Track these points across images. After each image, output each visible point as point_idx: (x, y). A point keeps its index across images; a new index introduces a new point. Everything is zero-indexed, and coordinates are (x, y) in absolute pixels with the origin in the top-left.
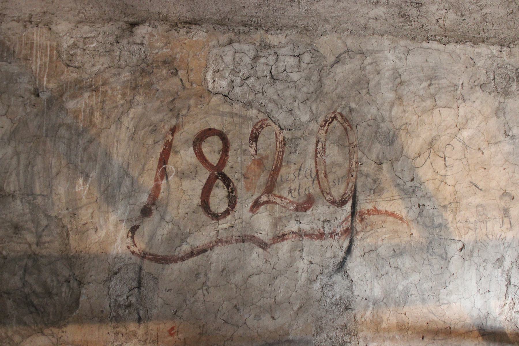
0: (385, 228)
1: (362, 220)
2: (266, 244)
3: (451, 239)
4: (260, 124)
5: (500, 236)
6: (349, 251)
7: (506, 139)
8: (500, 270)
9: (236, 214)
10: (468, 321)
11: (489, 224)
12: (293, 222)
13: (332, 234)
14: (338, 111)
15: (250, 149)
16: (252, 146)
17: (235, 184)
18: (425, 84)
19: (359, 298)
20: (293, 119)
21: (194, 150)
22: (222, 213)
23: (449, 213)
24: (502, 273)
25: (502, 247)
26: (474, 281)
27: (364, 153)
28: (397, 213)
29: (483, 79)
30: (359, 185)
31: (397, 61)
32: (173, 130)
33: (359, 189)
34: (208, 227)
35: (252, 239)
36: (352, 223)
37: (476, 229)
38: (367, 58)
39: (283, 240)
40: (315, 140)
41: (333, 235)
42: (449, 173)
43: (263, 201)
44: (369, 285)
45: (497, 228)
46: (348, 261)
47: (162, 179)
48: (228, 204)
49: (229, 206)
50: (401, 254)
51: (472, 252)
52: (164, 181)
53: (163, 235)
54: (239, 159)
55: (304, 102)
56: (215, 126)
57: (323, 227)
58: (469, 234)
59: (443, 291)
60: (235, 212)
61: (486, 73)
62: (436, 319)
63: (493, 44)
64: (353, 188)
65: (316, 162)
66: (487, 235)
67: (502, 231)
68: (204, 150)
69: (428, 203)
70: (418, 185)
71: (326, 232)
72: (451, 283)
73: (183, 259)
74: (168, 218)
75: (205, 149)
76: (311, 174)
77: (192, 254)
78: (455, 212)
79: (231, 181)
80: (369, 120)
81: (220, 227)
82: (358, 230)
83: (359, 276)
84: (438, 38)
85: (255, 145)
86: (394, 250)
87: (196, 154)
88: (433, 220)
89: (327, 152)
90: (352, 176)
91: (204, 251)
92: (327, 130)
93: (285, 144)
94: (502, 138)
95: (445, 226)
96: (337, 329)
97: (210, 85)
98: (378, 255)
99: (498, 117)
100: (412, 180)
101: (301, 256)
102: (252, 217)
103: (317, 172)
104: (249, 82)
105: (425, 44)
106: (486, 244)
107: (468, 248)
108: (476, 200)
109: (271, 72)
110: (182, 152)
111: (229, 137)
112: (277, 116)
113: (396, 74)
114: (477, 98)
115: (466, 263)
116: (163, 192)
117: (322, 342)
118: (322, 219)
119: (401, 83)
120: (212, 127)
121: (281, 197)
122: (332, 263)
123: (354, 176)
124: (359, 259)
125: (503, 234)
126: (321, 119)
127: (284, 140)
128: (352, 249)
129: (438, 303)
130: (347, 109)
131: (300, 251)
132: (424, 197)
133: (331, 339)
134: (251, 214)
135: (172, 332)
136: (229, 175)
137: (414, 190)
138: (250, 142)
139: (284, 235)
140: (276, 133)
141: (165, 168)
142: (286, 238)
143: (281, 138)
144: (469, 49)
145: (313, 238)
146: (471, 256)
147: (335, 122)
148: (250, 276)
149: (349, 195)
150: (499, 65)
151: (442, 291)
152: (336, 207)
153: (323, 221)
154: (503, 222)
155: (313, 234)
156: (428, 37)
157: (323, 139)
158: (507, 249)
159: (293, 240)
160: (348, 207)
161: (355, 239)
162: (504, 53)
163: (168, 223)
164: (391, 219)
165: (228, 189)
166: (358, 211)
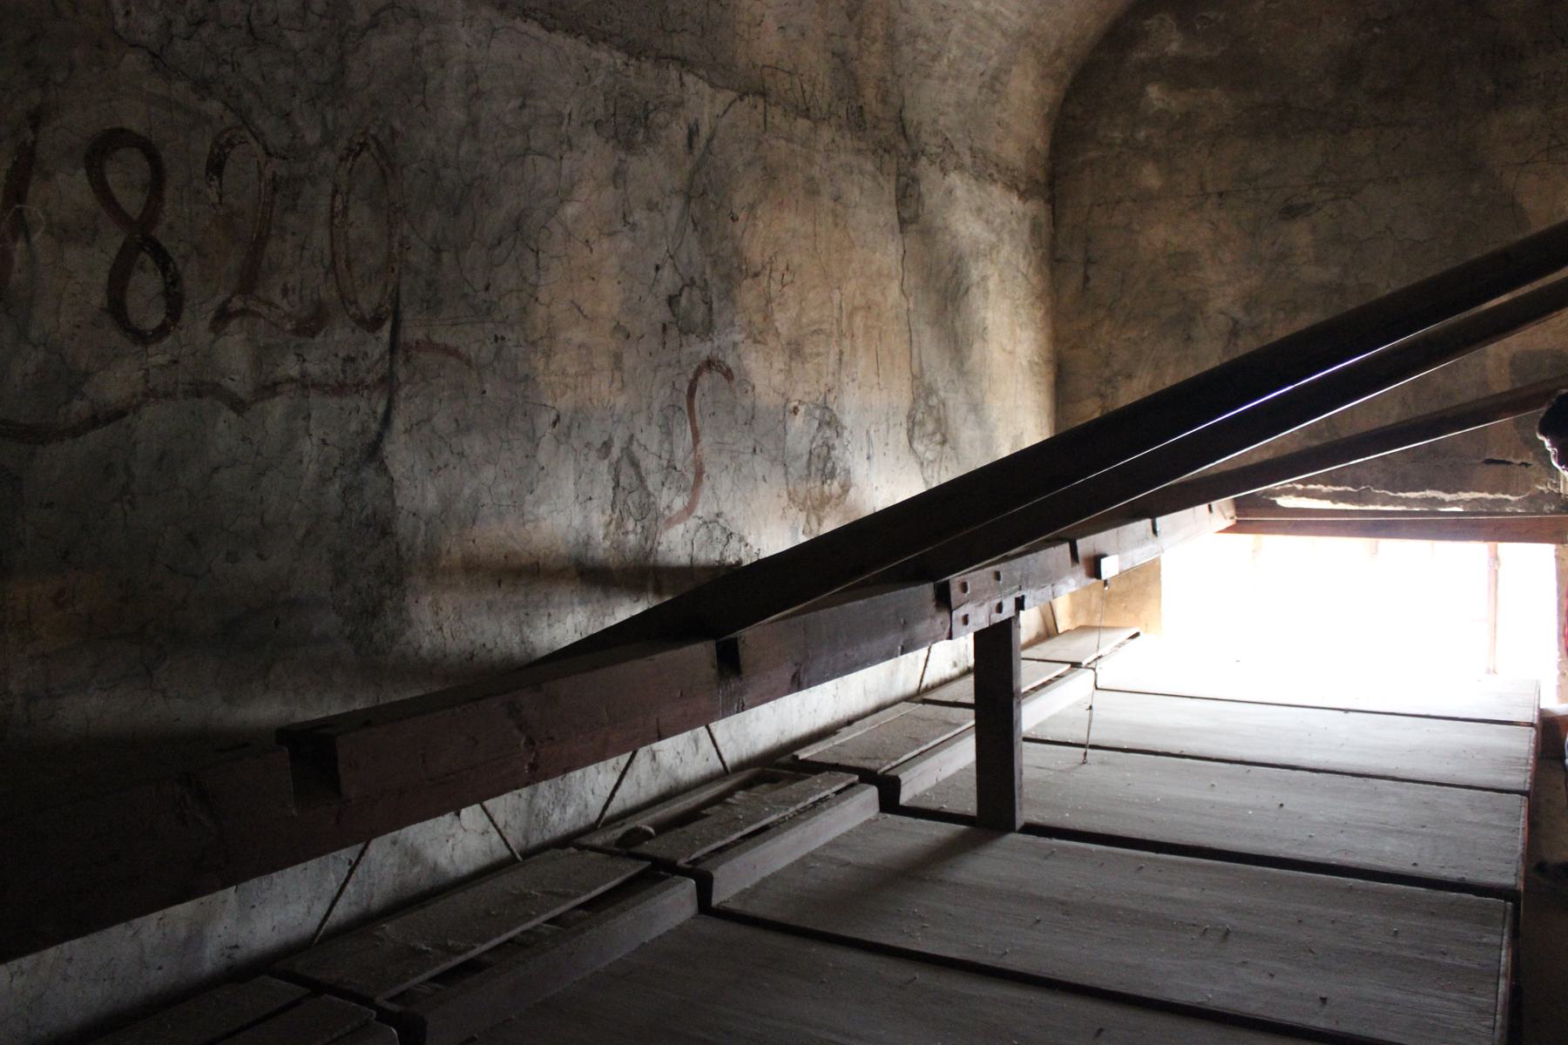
0: (444, 377)
1: (408, 360)
2: (242, 401)
3: (541, 405)
4: (227, 135)
5: (609, 401)
6: (386, 421)
7: (625, 229)
8: (606, 462)
9: (182, 333)
10: (563, 551)
11: (595, 380)
12: (292, 358)
13: (359, 386)
14: (372, 132)
15: (208, 190)
16: (212, 183)
17: (180, 267)
18: (514, 103)
19: (404, 512)
20: (291, 135)
21: (88, 174)
22: (154, 331)
23: (539, 355)
24: (609, 468)
25: (610, 421)
26: (571, 482)
27: (413, 227)
28: (463, 350)
29: (600, 112)
30: (404, 288)
31: (475, 47)
32: (36, 119)
33: (404, 299)
34: (127, 360)
35: (217, 391)
36: (391, 366)
37: (576, 387)
38: (426, 30)
39: (275, 394)
40: (329, 188)
41: (360, 387)
42: (542, 282)
43: (234, 309)
44: (419, 486)
45: (604, 388)
46: (385, 440)
47: (15, 239)
48: (165, 311)
49: (168, 315)
50: (469, 429)
51: (569, 428)
52: (20, 245)
53: (26, 375)
54: (187, 210)
55: (311, 102)
56: (134, 124)
57: (344, 371)
58: (567, 397)
59: (529, 498)
60: (181, 329)
61: (605, 100)
62: (518, 548)
63: (618, 49)
64: (394, 295)
65: (331, 234)
66: (590, 399)
67: (610, 392)
68: (109, 178)
69: (509, 335)
70: (496, 299)
71: (348, 381)
72: (540, 483)
73: (75, 432)
74: (34, 333)
75: (113, 178)
76: (322, 260)
77: (94, 421)
78: (548, 355)
79: (171, 260)
80: (422, 160)
81: (153, 360)
82: (401, 380)
83: (403, 470)
84: (540, 15)
85: (217, 183)
86: (456, 420)
87: (92, 185)
88: (517, 367)
89: (352, 215)
90: (393, 270)
91: (121, 414)
92: (351, 169)
93: (275, 190)
94: (619, 226)
95: (534, 379)
96: (370, 572)
97: (120, 22)
98: (433, 431)
99: (616, 187)
100: (487, 288)
101: (307, 429)
102: (214, 342)
103: (334, 254)
104: (206, 31)
105: (518, 22)
106: (589, 416)
107: (565, 420)
108: (578, 335)
109: (249, 20)
110: (60, 177)
111: (164, 155)
112: (260, 122)
113: (471, 77)
114: (589, 146)
115: (562, 447)
116: (20, 272)
117: (345, 601)
118: (341, 355)
119: (478, 94)
120: (126, 126)
121: (270, 304)
122: (360, 444)
123: (396, 272)
124: (403, 438)
125: (612, 399)
126: (342, 143)
127: (274, 179)
128: (392, 416)
129: (521, 521)
130: (387, 131)
131: (304, 418)
132: (504, 322)
133: (359, 594)
134: (212, 336)
135: (62, 600)
136: (165, 244)
137: (489, 309)
138: (207, 174)
139: (275, 384)
140: (258, 162)
141: (20, 211)
142: (278, 390)
143: (268, 174)
144: (584, 48)
145: (327, 392)
146: (568, 436)
147: (365, 154)
148: (216, 469)
149: (387, 309)
150: (623, 90)
151: (526, 498)
152: (365, 332)
153: (344, 359)
154: (613, 378)
155: (327, 385)
156: (524, 10)
157: (344, 188)
158: (616, 425)
159: (292, 394)
160: (385, 333)
161: (396, 398)
162: (632, 68)
163: (35, 346)
164: (453, 361)
165: (164, 274)
166: (402, 341)
